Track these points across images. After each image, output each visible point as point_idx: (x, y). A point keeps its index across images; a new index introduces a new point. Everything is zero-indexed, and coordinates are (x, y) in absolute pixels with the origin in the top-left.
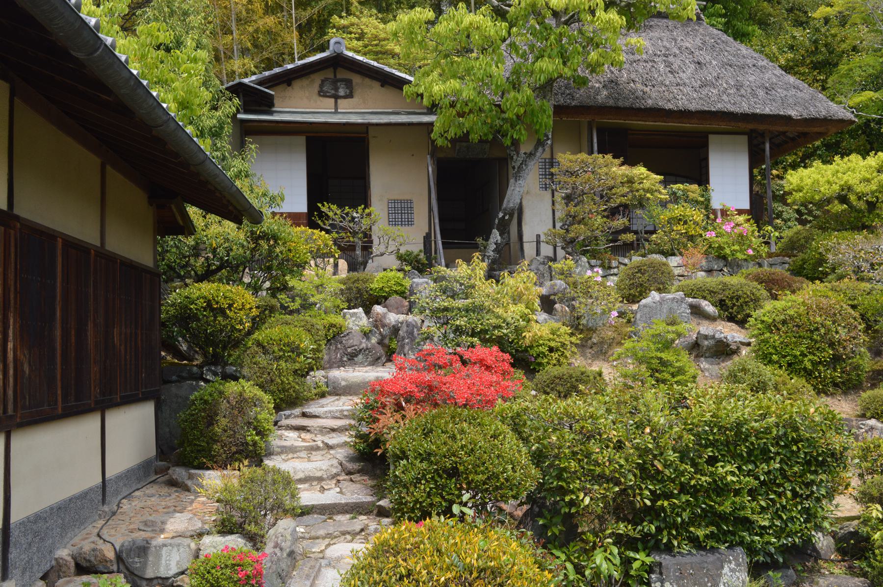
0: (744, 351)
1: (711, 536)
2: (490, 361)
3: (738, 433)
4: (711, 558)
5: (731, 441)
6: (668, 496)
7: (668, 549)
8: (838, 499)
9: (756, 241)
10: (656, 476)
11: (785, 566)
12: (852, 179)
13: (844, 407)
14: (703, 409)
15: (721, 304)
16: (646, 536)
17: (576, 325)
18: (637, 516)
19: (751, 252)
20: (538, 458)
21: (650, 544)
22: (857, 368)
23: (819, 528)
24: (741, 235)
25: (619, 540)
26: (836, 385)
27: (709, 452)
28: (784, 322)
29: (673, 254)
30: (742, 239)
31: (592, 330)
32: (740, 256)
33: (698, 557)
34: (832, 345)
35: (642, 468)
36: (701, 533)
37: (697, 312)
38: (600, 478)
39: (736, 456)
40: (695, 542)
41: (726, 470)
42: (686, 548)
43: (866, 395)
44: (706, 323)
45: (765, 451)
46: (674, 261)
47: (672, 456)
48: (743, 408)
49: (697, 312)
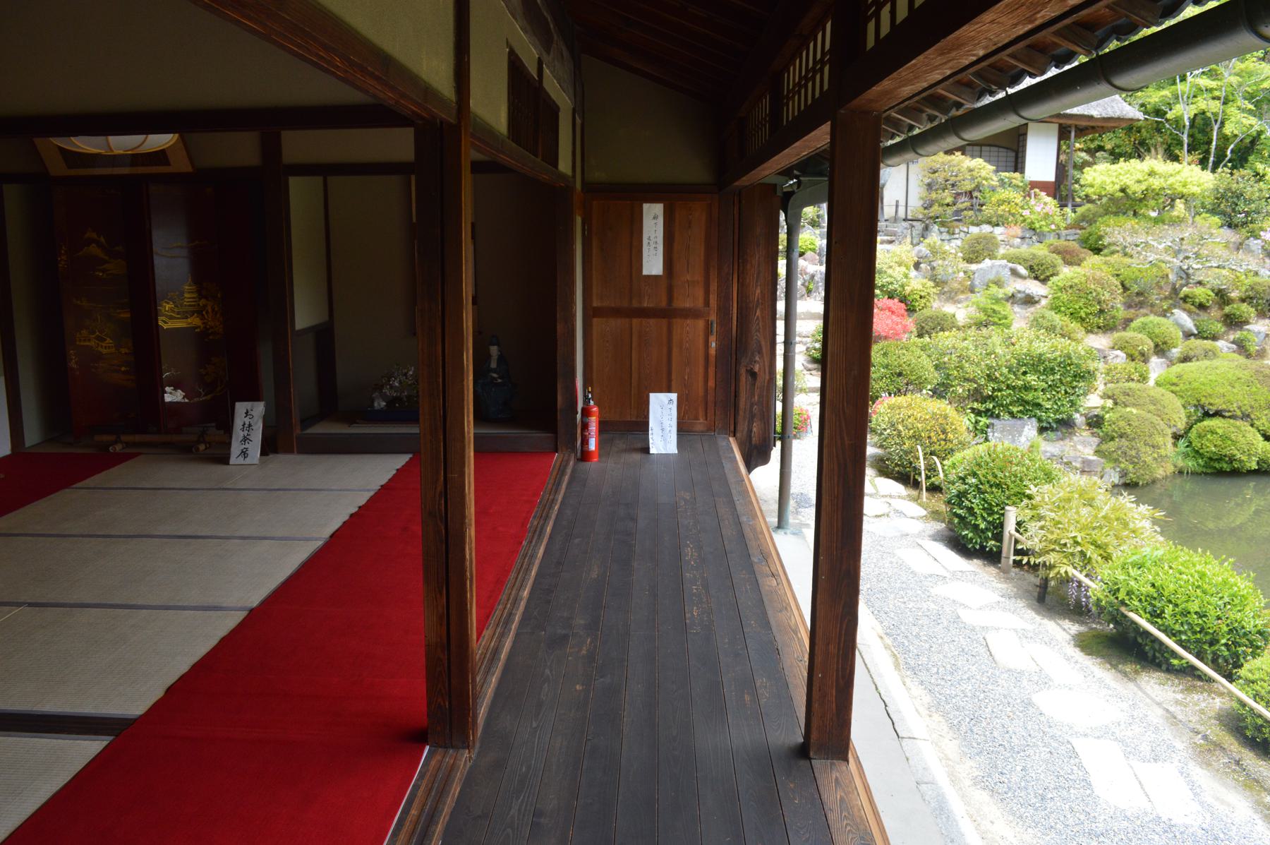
0: (1044, 302)
1: (1020, 412)
2: (894, 308)
3: (1040, 359)
4: (1019, 422)
5: (1037, 364)
6: (1000, 390)
7: (998, 416)
8: (1090, 396)
9: (1058, 219)
10: (995, 380)
11: (1057, 430)
12: (1129, 181)
13: (1099, 342)
14: (1022, 347)
15: (1031, 268)
16: (988, 410)
17: (933, 278)
18: (984, 399)
19: (1053, 227)
20: (937, 367)
21: (989, 413)
22: (1113, 317)
23: (1077, 411)
24: (1047, 214)
25: (973, 410)
26: (1099, 328)
27: (1023, 369)
28: (1071, 287)
29: (998, 225)
30: (1047, 216)
31: (945, 282)
32: (1045, 229)
33: (1013, 421)
34: (1099, 303)
35: (988, 375)
36: (1015, 409)
37: (1014, 273)
38: (968, 380)
39: (1037, 371)
40: (1012, 415)
41: (1031, 378)
42: (1007, 417)
43: (1116, 335)
44: (1019, 280)
45: (1052, 369)
46: (998, 231)
47: (1005, 371)
48: (1045, 346)
49: (1014, 273)
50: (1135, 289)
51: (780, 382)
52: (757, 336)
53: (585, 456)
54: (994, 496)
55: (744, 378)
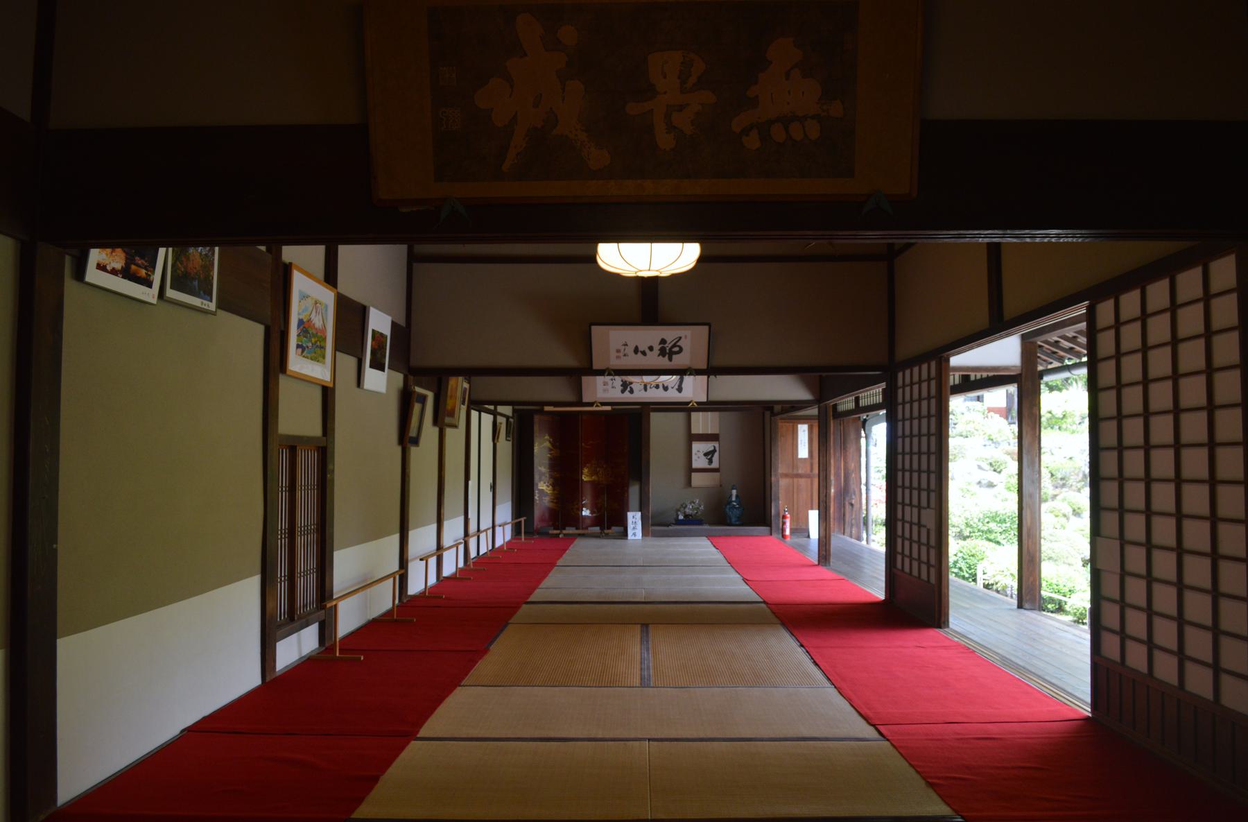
10: (971, 526)
37: (980, 467)
41: (992, 525)
50: (1059, 476)
51: (864, 507)
52: (853, 486)
53: (784, 536)
54: (972, 561)
55: (848, 507)
